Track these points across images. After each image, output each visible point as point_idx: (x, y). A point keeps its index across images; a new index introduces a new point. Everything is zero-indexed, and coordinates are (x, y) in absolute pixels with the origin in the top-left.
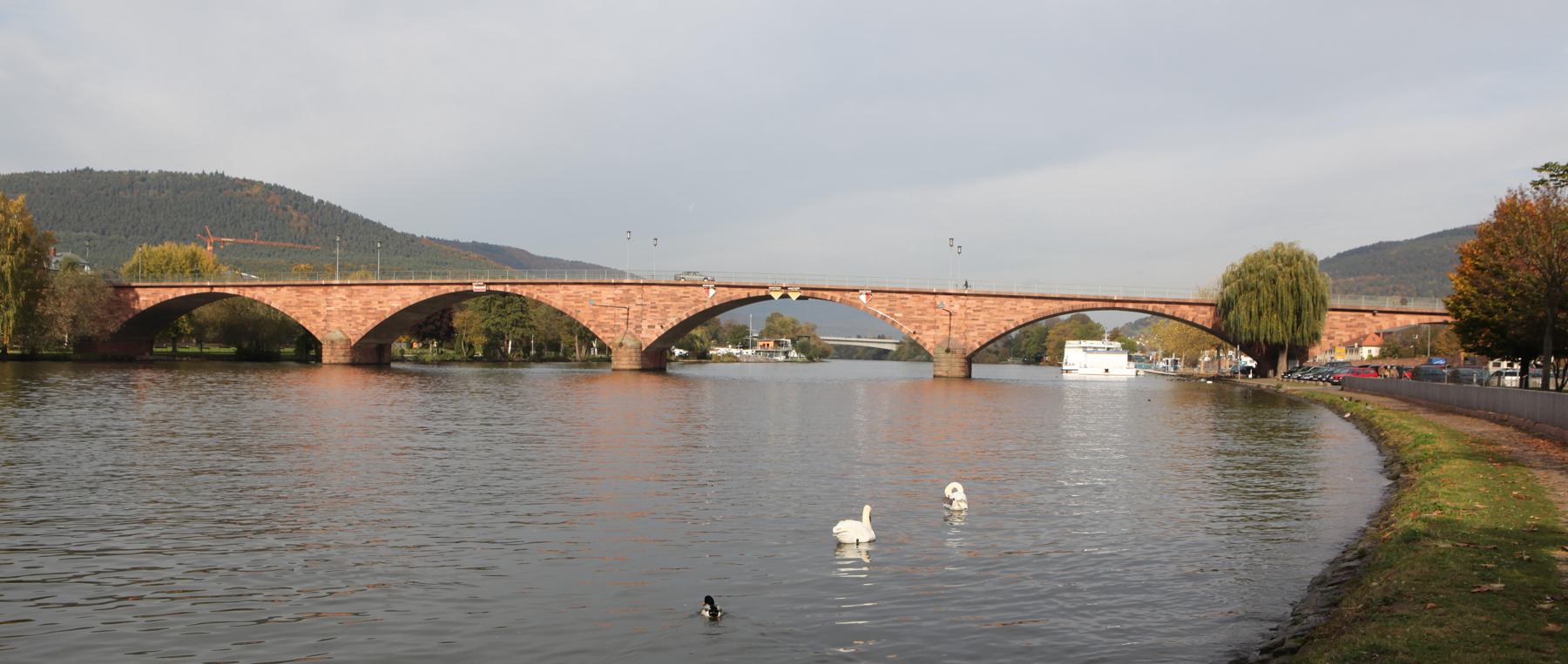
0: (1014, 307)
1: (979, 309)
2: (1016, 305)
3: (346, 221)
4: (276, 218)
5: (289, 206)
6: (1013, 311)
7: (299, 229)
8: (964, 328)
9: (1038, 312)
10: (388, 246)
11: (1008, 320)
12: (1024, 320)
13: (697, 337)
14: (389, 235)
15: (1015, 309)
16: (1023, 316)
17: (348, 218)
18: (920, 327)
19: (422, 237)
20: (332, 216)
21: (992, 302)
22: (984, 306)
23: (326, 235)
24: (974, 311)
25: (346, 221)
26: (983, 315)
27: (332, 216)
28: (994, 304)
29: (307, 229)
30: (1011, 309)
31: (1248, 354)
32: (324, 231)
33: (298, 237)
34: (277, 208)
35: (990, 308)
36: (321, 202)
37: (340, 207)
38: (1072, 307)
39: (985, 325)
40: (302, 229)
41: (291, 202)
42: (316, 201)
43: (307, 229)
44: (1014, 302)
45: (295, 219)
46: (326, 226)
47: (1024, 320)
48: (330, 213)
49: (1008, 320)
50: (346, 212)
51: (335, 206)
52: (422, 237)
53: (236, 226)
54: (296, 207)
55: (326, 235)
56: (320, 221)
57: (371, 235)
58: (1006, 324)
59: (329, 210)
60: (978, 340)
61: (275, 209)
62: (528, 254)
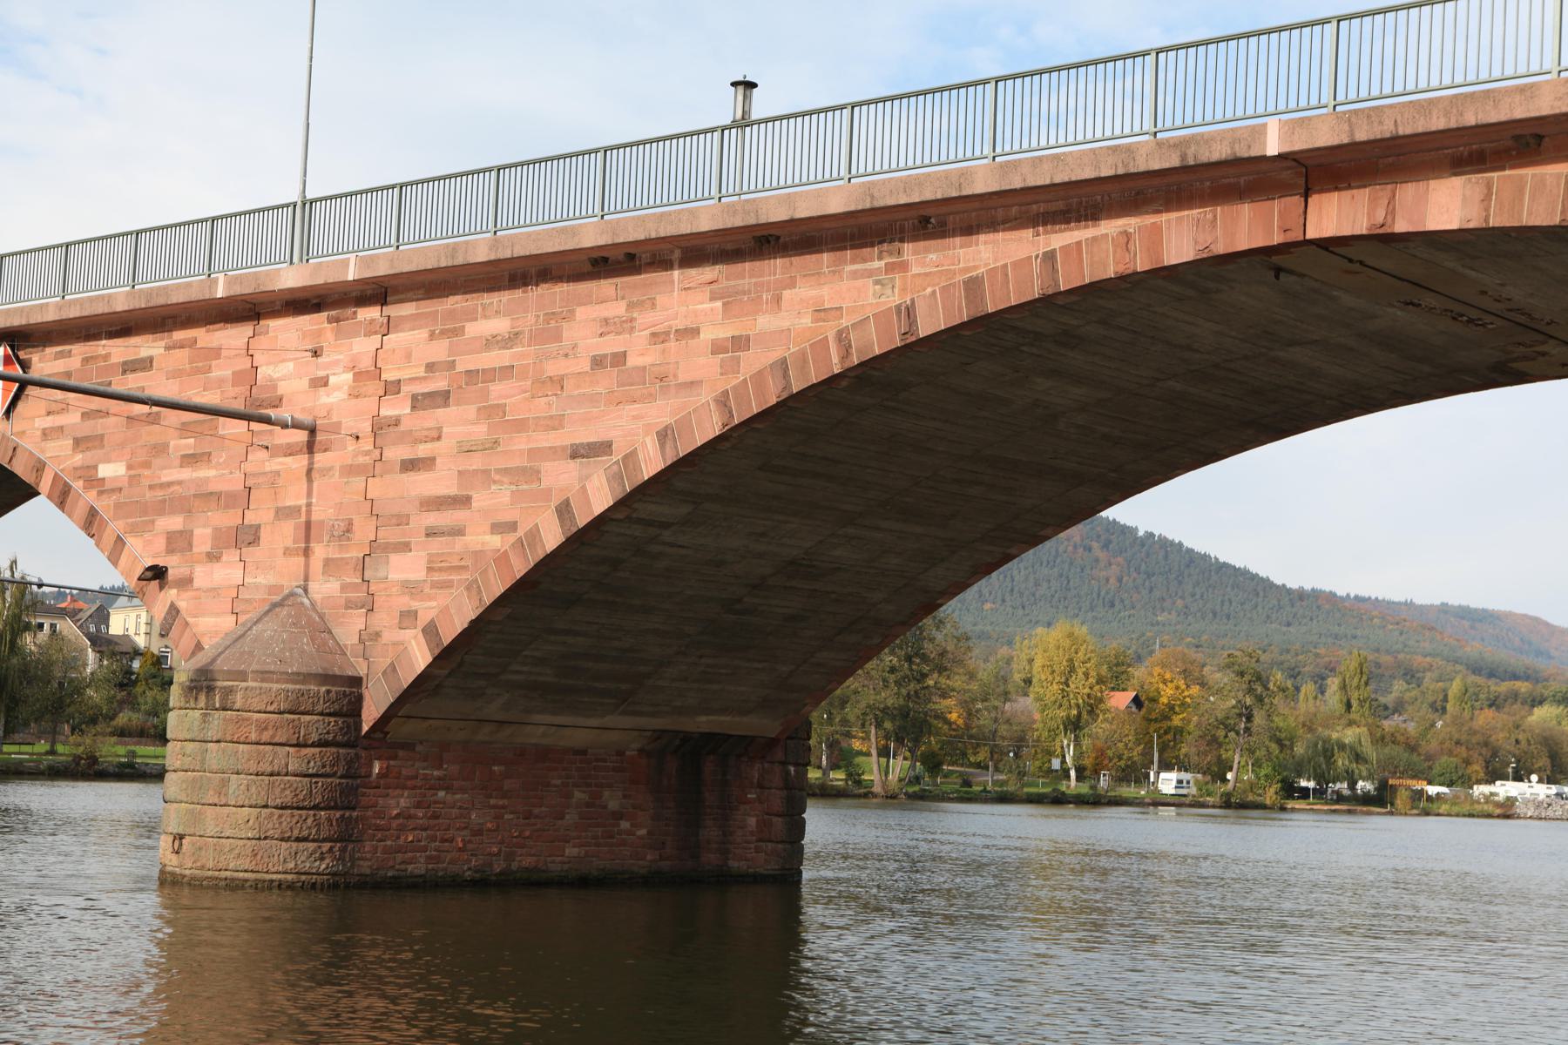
0: (611, 345)
1: (439, 384)
2: (627, 326)
3: (1188, 566)
4: (1071, 564)
5: (1095, 545)
6: (606, 381)
7: (1107, 580)
8: (364, 531)
9: (754, 361)
10: (1256, 606)
11: (576, 453)
12: (663, 435)
13: (1342, 747)
14: (1259, 588)
15: (620, 359)
16: (662, 412)
17: (1192, 561)
18: (179, 541)
19: (1348, 595)
20: (1166, 558)
21: (499, 325)
22: (465, 363)
23: (1151, 590)
24: (417, 402)
25: (1188, 566)
26: (459, 423)
27: (1166, 558)
28: (512, 339)
29: (1120, 580)
30: (598, 362)
31: (821, 702)
32: (1147, 583)
33: (1103, 593)
34: (1075, 547)
35: (490, 375)
36: (1150, 535)
37: (1180, 544)
38: (973, 286)
39: (463, 501)
40: (1112, 581)
41: (1099, 536)
42: (1141, 533)
43: (1120, 580)
44: (617, 309)
45: (1102, 565)
46: (1154, 575)
47: (663, 435)
48: (1162, 553)
49: (576, 453)
50: (1190, 551)
51: (1172, 543)
52: (1348, 595)
53: (1005, 577)
54: (1106, 546)
55: (1151, 590)
56: (1143, 567)
57: (1229, 589)
58: (562, 476)
59: (1161, 548)
60: (428, 610)
61: (1070, 548)
62: (1547, 624)
